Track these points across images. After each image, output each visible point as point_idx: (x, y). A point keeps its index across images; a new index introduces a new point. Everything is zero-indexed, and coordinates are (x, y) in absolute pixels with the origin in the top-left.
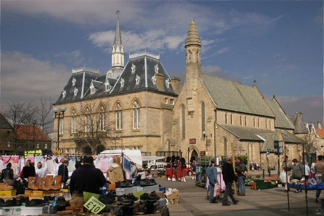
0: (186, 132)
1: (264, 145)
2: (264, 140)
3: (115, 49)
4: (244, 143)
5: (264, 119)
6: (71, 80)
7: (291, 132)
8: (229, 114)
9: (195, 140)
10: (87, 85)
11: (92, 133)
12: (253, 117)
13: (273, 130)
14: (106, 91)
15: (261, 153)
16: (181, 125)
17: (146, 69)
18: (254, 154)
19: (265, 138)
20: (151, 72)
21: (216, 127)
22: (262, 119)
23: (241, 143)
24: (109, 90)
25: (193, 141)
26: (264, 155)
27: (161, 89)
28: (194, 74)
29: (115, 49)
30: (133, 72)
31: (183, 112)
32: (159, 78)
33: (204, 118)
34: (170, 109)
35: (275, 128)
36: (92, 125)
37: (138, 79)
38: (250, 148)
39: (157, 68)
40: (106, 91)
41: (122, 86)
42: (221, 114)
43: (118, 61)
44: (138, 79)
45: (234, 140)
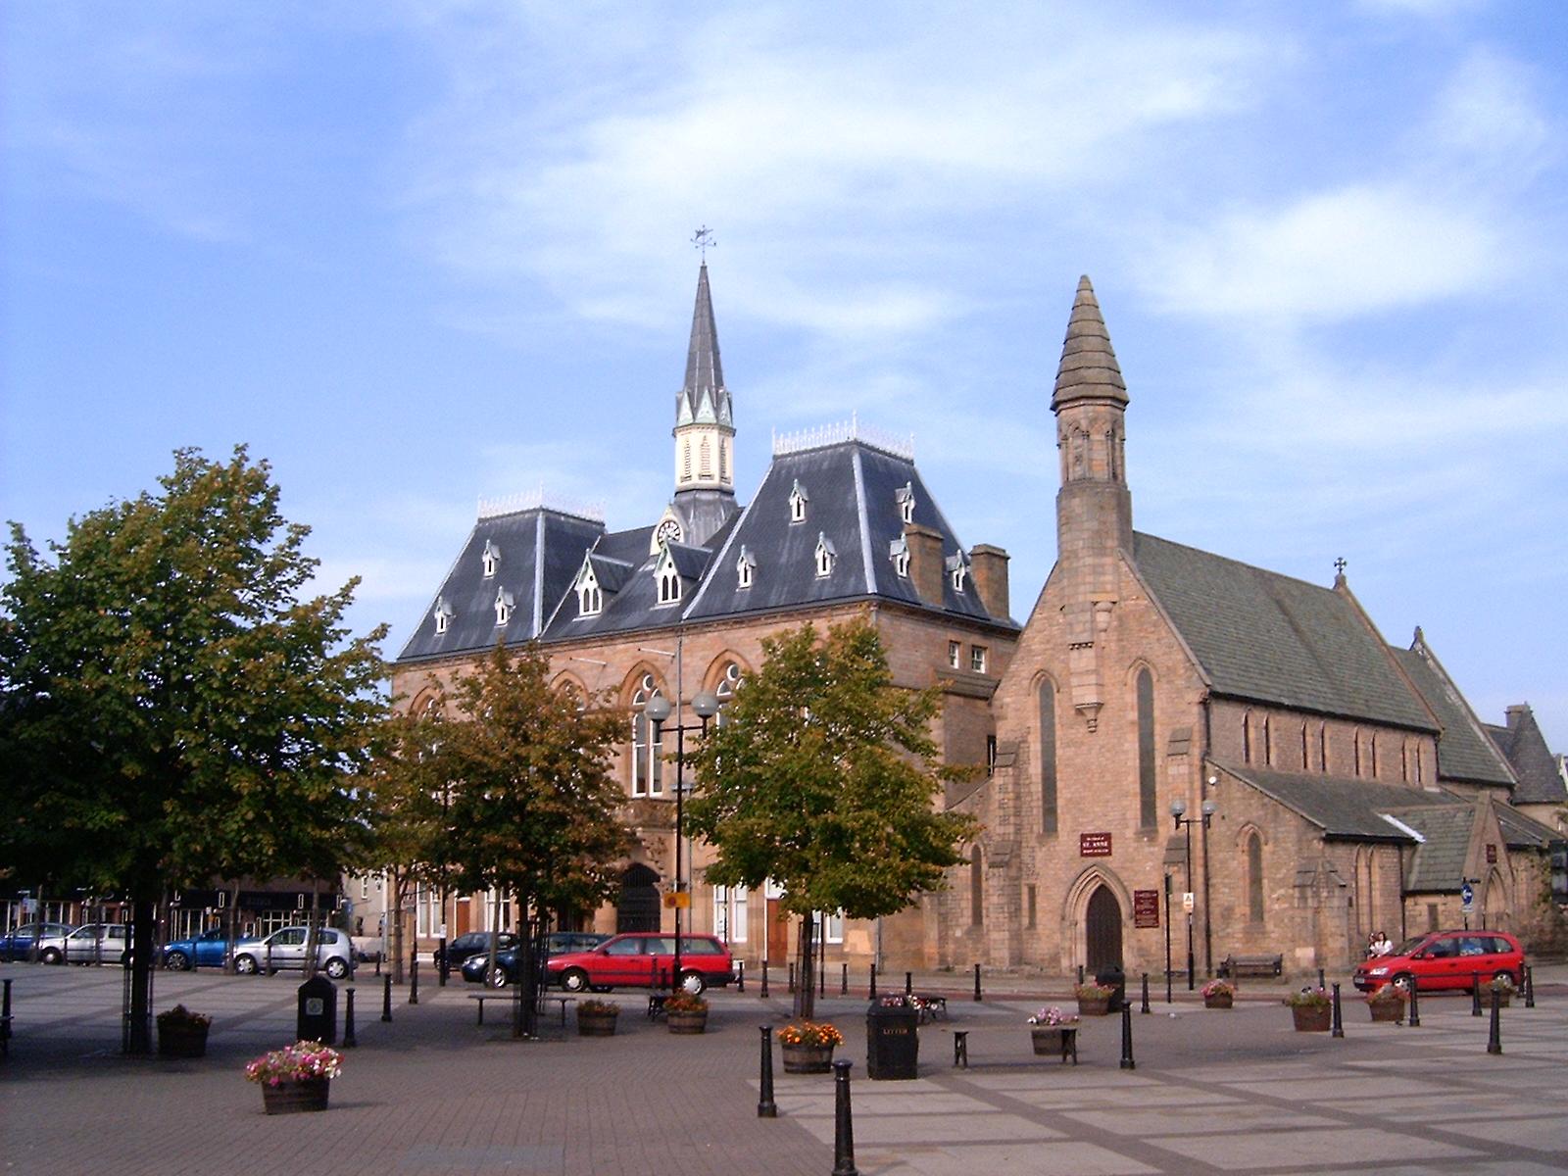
0: (1060, 802)
1: (1417, 861)
2: (1418, 837)
3: (694, 410)
4: (1341, 851)
5: (1393, 739)
6: (475, 549)
7: (1502, 796)
8: (1259, 717)
9: (1108, 837)
10: (560, 575)
11: (1339, 917)
12: (1353, 730)
13: (1433, 789)
14: (661, 604)
15: (1406, 894)
16: (1035, 769)
17: (862, 506)
18: (1378, 900)
19: (1416, 829)
20: (886, 525)
21: (1212, 780)
22: (1387, 740)
23: (1328, 850)
24: (673, 603)
25: (1097, 845)
26: (1419, 907)
27: (931, 600)
28: (1098, 534)
29: (694, 410)
30: (797, 517)
31: (1047, 709)
32: (923, 546)
33: (1152, 735)
34: (981, 694)
35: (1441, 779)
36: (1446, 880)
37: (823, 552)
38: (1363, 872)
39: (907, 504)
40: (661, 604)
41: (745, 583)
42: (1227, 716)
43: (688, 465)
44: (823, 552)
45: (1300, 840)
